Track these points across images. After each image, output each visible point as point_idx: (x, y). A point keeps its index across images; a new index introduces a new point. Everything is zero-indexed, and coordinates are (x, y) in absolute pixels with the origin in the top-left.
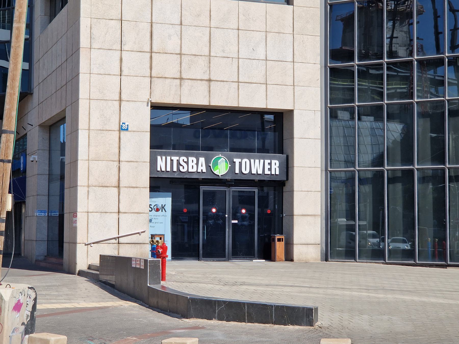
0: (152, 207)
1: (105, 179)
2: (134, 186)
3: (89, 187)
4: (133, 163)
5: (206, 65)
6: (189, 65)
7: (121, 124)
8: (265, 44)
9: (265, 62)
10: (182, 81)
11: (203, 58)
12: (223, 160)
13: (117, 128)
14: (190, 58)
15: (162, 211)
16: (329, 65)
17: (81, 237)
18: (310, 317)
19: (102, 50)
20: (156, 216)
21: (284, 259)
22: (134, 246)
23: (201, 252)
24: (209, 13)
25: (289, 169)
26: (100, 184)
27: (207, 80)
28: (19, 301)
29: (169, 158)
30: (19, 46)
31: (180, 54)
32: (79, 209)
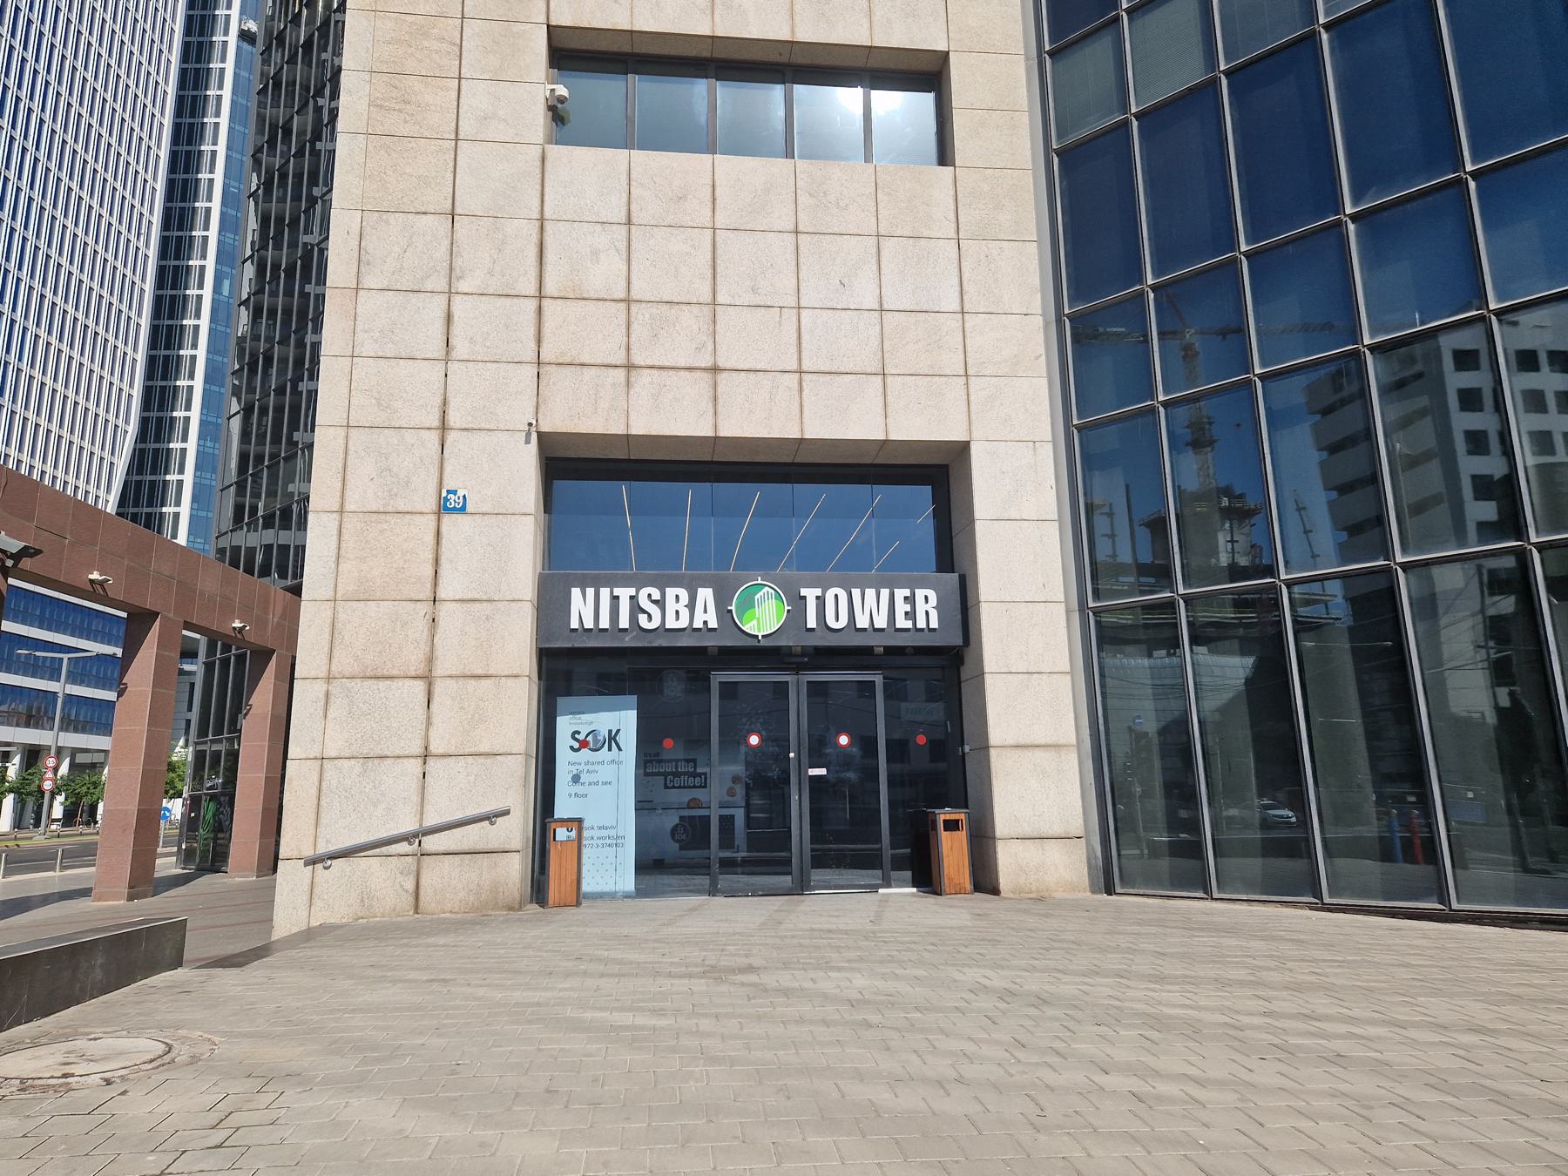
1: (384, 654)
2: (480, 672)
3: (331, 680)
4: (477, 605)
5: (702, 330)
6: (652, 328)
7: (444, 494)
8: (875, 267)
9: (877, 314)
10: (634, 373)
11: (695, 309)
12: (768, 592)
13: (431, 504)
14: (655, 310)
15: (610, 749)
19: (390, 293)
20: (593, 764)
21: (969, 886)
22: (470, 860)
24: (710, 190)
25: (971, 612)
26: (369, 670)
31: (628, 301)
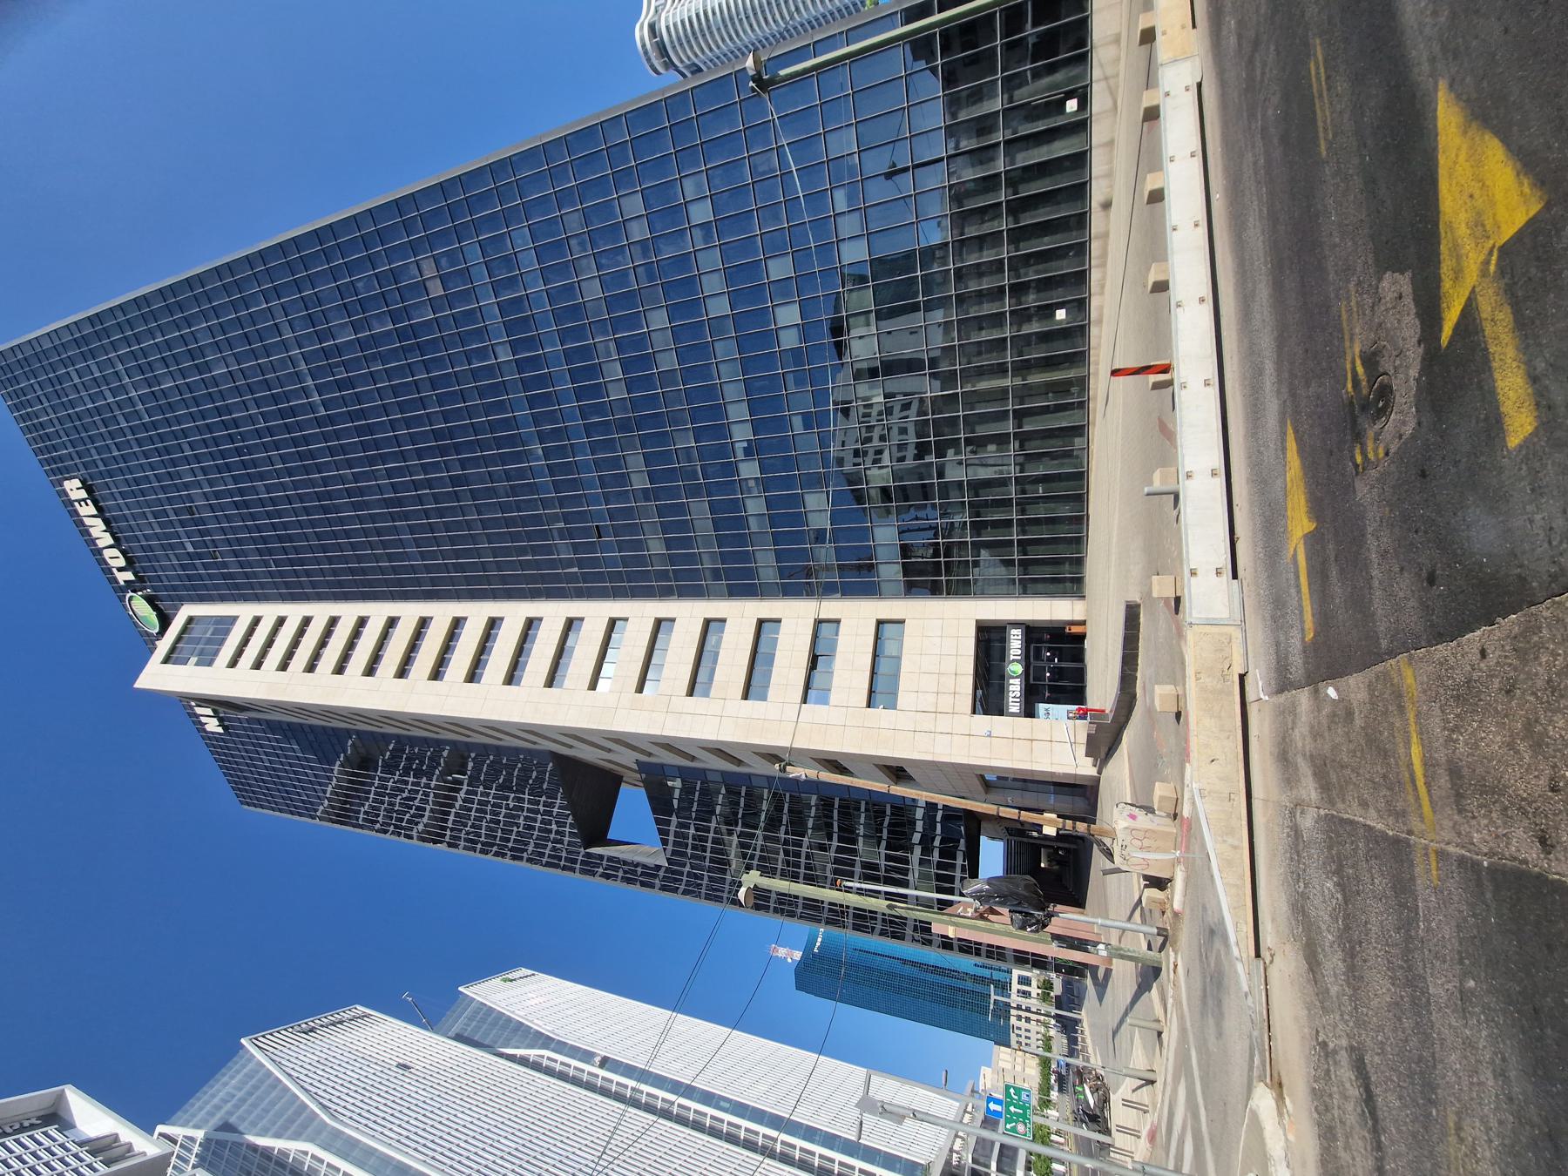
17: (1072, 771)
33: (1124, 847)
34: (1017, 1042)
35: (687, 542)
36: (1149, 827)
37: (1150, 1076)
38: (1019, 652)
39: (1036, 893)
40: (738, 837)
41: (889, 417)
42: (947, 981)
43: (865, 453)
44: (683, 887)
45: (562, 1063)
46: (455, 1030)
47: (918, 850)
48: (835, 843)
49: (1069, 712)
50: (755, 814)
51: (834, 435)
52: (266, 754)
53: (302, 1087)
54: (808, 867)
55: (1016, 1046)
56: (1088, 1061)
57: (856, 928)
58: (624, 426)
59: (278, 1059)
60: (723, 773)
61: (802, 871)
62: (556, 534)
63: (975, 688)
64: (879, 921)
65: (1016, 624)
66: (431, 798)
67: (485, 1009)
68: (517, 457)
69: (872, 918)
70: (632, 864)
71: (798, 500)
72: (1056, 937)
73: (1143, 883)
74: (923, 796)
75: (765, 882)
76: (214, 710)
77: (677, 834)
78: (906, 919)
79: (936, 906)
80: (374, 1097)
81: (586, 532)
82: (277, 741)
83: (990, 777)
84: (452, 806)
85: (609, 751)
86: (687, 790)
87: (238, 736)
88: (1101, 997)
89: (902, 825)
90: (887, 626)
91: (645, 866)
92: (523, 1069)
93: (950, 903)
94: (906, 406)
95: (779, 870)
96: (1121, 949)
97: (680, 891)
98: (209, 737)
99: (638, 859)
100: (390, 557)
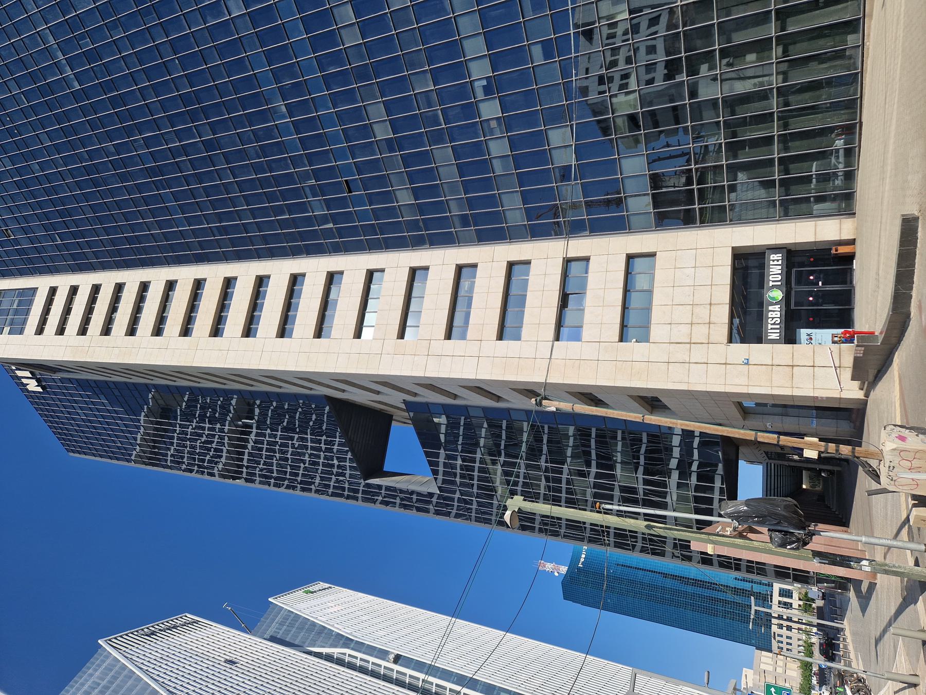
0: (808, 343)
13: (746, 366)
16: (698, 225)
17: (836, 395)
18: (910, 219)
23: (847, 307)
27: (710, 306)
28: (896, 437)
29: (769, 331)
30: (694, 425)
31: (692, 324)
32: (812, 395)
33: (891, 468)
34: (779, 648)
35: (434, 191)
36: (920, 448)
37: (913, 680)
38: (780, 277)
39: (796, 513)
40: (502, 466)
41: (635, 36)
42: (707, 593)
43: (611, 79)
44: (454, 511)
45: (361, 660)
46: (268, 635)
47: (675, 475)
48: (594, 470)
49: (834, 336)
50: (515, 445)
51: (576, 63)
52: (81, 408)
53: (151, 677)
54: (569, 492)
55: (777, 651)
56: (850, 666)
57: (618, 545)
58: (362, 74)
59: (130, 656)
60: (485, 409)
61: (564, 495)
62: (308, 190)
63: (732, 317)
64: (640, 540)
65: (775, 249)
66: (226, 440)
67: (293, 615)
68: (263, 116)
69: (632, 537)
70: (407, 492)
71: (540, 138)
72: (817, 554)
73: (911, 502)
74: (679, 424)
75: (529, 506)
76: (31, 373)
77: (445, 465)
78: (665, 537)
79: (695, 526)
80: (209, 686)
81: (336, 187)
82: (88, 396)
83: (747, 404)
84: (245, 447)
85: (378, 393)
86: (453, 425)
87: (55, 394)
88: (864, 609)
89: (658, 451)
90: (637, 260)
91: (419, 494)
92: (330, 664)
93: (709, 523)
94: (654, 21)
95: (542, 496)
96: (886, 565)
97: (453, 514)
98: (31, 395)
99: (412, 487)
100: (160, 225)
